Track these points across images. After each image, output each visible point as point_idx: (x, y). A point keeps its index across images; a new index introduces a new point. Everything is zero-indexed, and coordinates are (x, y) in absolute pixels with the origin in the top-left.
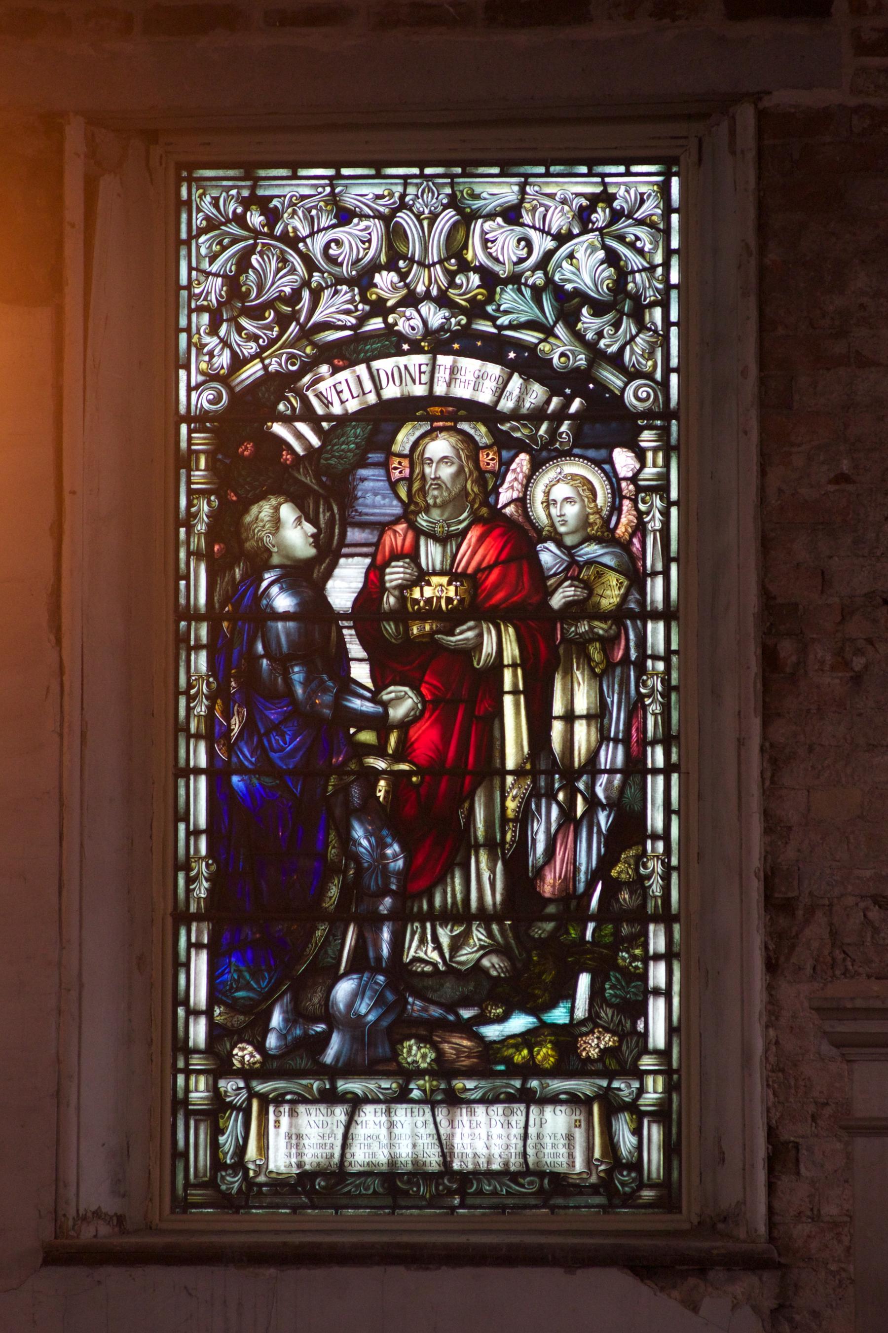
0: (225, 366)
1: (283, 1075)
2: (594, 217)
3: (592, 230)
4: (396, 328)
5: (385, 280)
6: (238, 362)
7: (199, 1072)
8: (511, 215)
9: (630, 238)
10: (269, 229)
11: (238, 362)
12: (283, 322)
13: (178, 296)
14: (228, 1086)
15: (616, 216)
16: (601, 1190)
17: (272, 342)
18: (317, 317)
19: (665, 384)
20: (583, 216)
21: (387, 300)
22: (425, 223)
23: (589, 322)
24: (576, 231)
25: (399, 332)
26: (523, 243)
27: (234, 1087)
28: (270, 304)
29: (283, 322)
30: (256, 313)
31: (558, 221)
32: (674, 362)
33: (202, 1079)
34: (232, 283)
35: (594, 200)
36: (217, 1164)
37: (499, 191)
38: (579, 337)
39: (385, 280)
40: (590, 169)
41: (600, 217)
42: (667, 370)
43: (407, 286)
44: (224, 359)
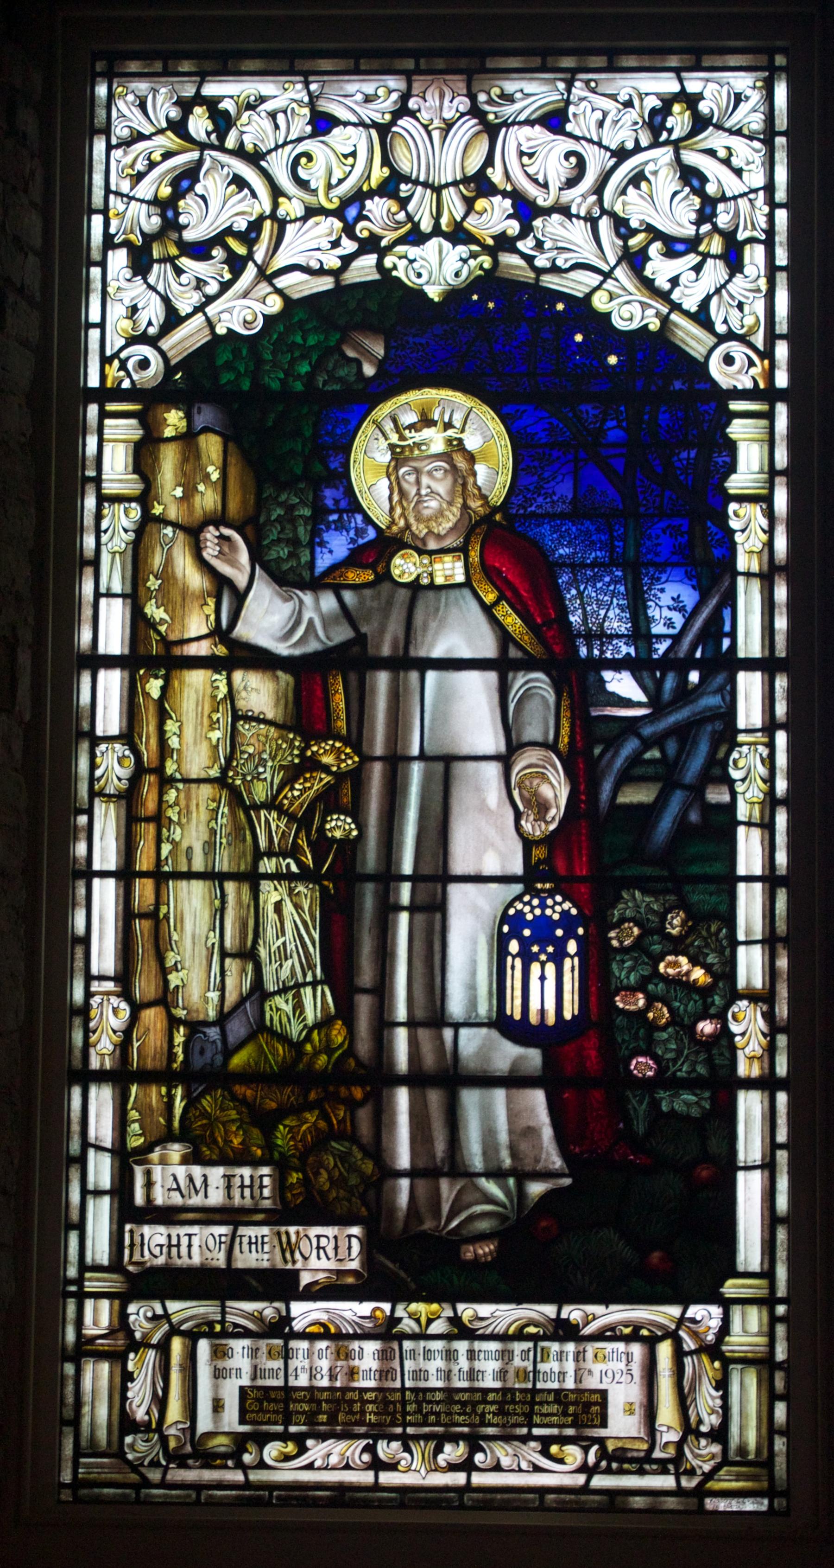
0: (154, 321)
1: (352, 936)
2: (670, 122)
3: (667, 143)
4: (394, 273)
5: (378, 207)
6: (173, 319)
7: (97, 1296)
8: (554, 120)
9: (722, 153)
10: (218, 137)
11: (173, 319)
12: (236, 264)
13: (598, 52)
14: (139, 1314)
15: (700, 123)
16: (671, 1467)
17: (225, 287)
18: (280, 262)
19: (768, 354)
20: (656, 122)
21: (382, 238)
22: (436, 135)
23: (660, 269)
24: (644, 143)
25: (398, 279)
26: (573, 160)
27: (149, 1314)
28: (219, 239)
29: (236, 264)
30: (200, 251)
31: (621, 134)
32: (782, 327)
33: (105, 1304)
34: (167, 207)
35: (668, 102)
36: (125, 1423)
37: (536, 92)
38: (648, 284)
39: (378, 207)
40: (73, 1227)
41: (679, 121)
42: (771, 337)
43: (409, 218)
44: (152, 312)
